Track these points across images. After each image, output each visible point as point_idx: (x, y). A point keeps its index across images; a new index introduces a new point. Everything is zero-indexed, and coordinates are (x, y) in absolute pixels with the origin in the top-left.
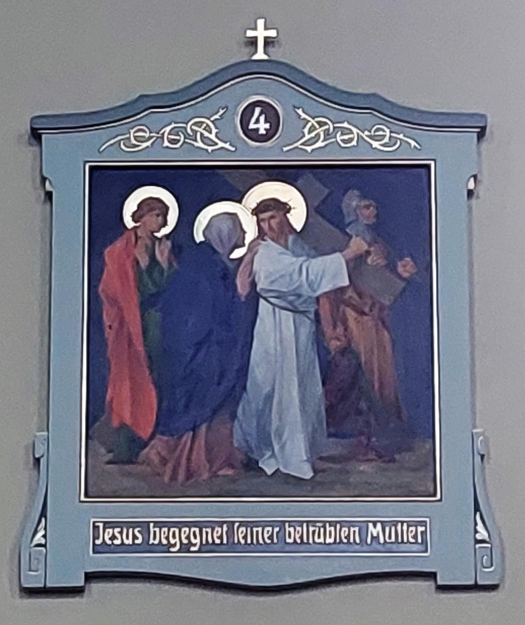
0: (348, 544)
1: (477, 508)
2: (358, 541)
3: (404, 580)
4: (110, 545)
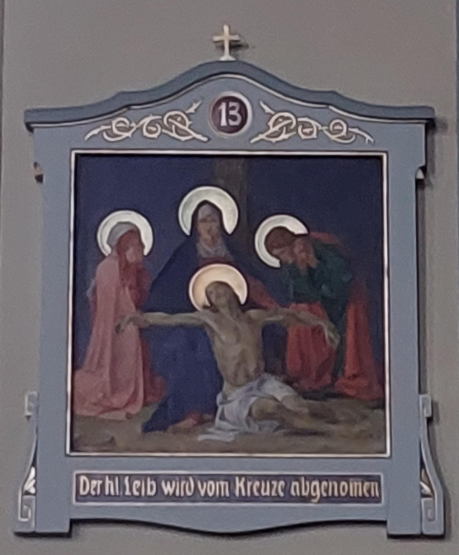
1: (34, 464)
4: (258, 497)
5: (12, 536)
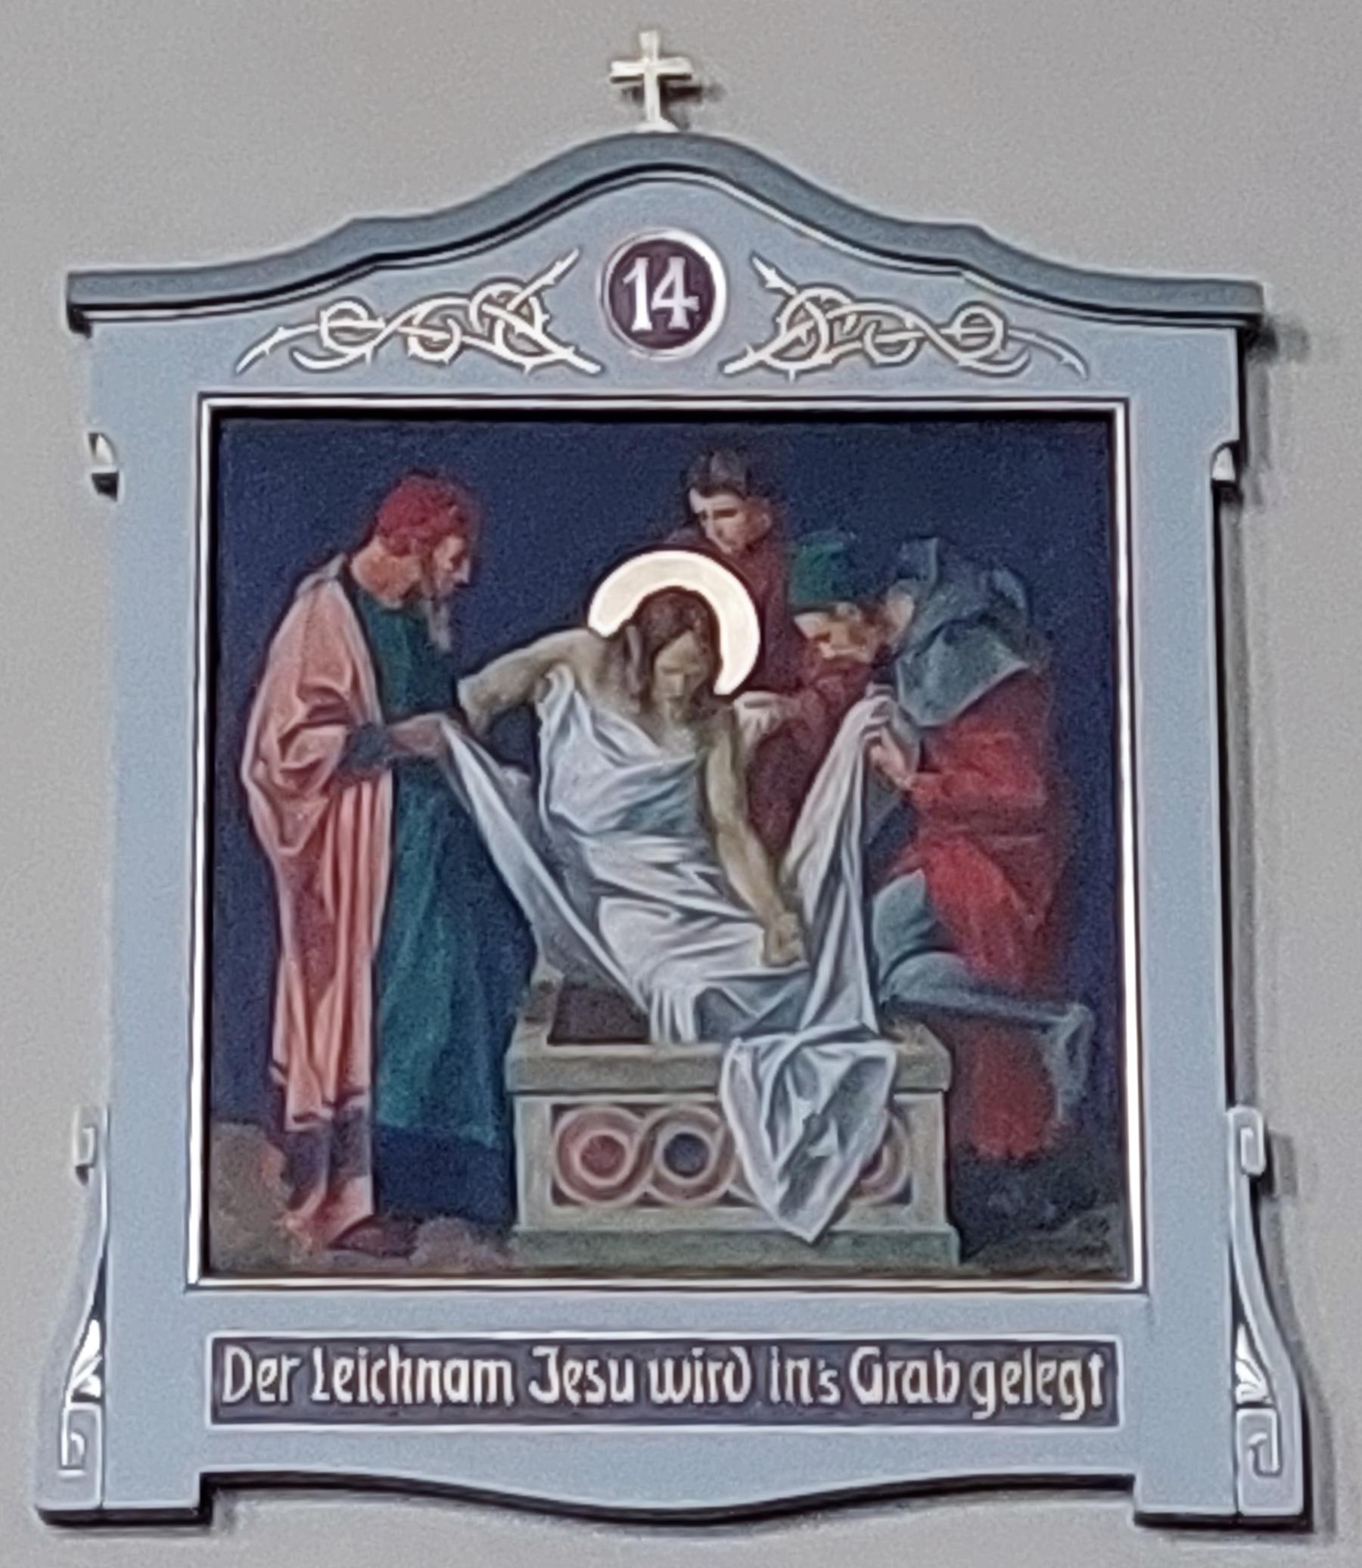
0: (371, 1406)
1: (98, 1311)
2: (509, 1396)
3: (621, 1529)
5: (35, 1517)
